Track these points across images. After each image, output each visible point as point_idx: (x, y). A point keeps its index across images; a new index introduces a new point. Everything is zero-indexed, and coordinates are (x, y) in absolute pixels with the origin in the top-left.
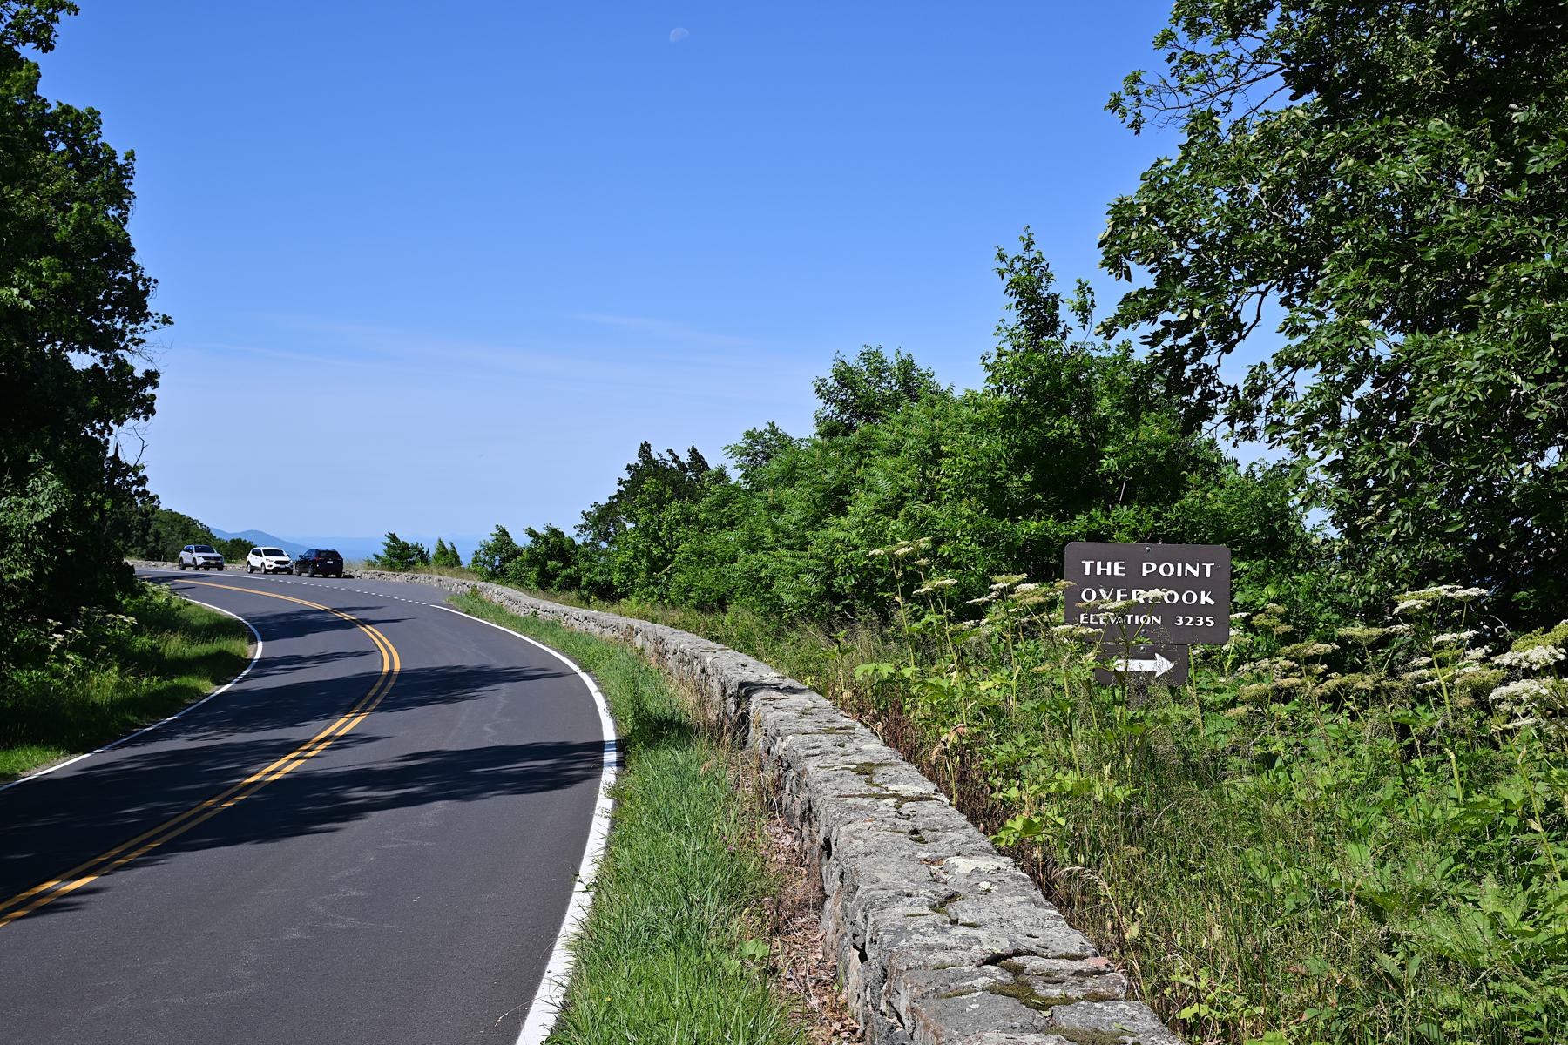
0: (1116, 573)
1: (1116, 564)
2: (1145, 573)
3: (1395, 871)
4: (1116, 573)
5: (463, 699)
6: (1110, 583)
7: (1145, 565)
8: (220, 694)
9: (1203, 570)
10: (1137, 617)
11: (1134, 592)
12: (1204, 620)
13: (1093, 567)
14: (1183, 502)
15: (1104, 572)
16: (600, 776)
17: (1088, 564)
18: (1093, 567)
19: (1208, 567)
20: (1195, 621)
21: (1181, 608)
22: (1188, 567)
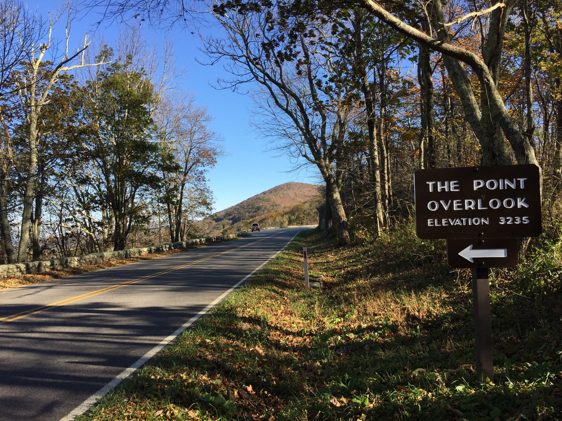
0: (451, 190)
1: (451, 183)
2: (475, 188)
3: (139, 88)
4: (451, 190)
5: (184, 307)
6: (447, 196)
7: (475, 182)
8: (4, 317)
9: (518, 183)
10: (470, 220)
11: (466, 201)
12: (521, 220)
13: (435, 186)
14: (507, 111)
15: (443, 184)
16: (161, 350)
17: (431, 184)
18: (435, 186)
19: (522, 180)
20: (514, 220)
21: (503, 212)
22: (507, 182)
